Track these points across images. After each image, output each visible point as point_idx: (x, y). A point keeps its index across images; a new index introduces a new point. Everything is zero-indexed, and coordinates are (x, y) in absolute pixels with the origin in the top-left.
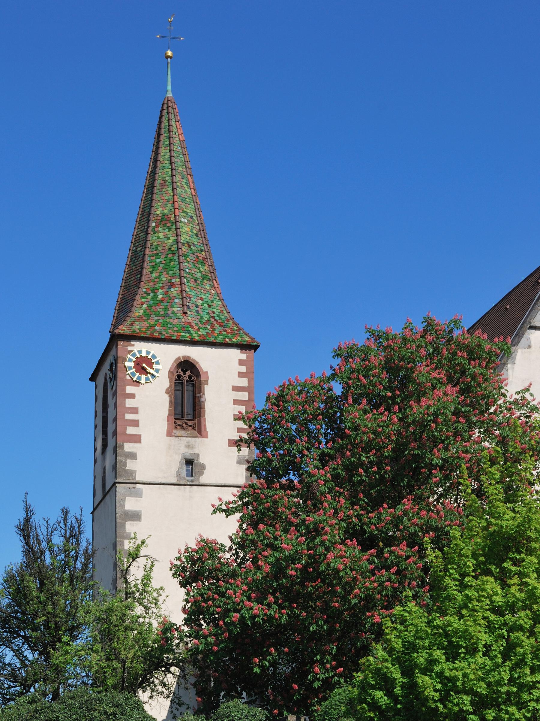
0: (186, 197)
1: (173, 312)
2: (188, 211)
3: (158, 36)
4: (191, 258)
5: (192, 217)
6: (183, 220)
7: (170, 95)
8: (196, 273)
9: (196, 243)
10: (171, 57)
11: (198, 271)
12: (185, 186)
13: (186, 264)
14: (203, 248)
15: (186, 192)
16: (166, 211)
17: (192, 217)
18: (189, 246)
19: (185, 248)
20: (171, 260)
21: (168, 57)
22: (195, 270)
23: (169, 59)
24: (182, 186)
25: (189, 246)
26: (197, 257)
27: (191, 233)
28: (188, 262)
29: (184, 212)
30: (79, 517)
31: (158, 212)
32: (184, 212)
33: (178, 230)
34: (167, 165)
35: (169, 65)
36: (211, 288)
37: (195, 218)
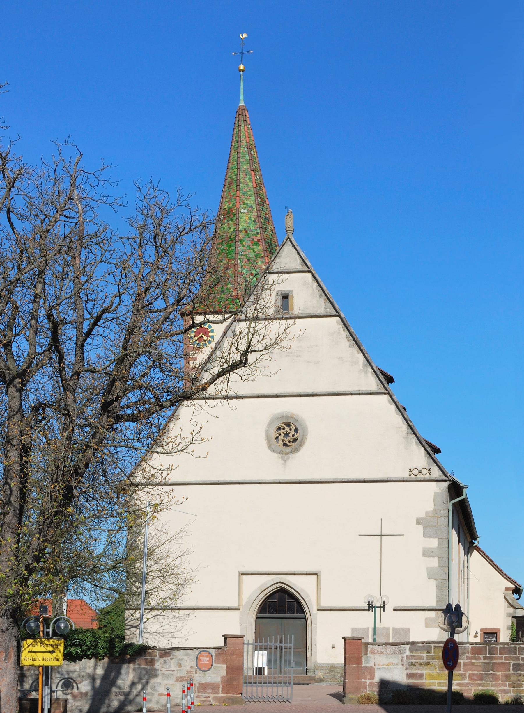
0: (248, 190)
1: (227, 289)
2: (248, 202)
3: (251, 52)
4: (247, 242)
5: (251, 207)
6: (242, 211)
7: (242, 103)
8: (250, 254)
9: (252, 228)
10: (243, 71)
11: (252, 251)
12: (248, 181)
13: (242, 247)
14: (259, 231)
15: (248, 186)
16: (231, 205)
17: (251, 207)
18: (246, 232)
19: (241, 235)
20: (230, 246)
21: (240, 71)
22: (249, 251)
23: (242, 72)
24: (245, 182)
25: (246, 232)
26: (253, 240)
27: (249, 221)
28: (243, 246)
29: (244, 203)
30: (173, 468)
31: (226, 207)
32: (244, 203)
33: (237, 220)
34: (235, 166)
35: (242, 77)
36: (262, 264)
37: (254, 207)
